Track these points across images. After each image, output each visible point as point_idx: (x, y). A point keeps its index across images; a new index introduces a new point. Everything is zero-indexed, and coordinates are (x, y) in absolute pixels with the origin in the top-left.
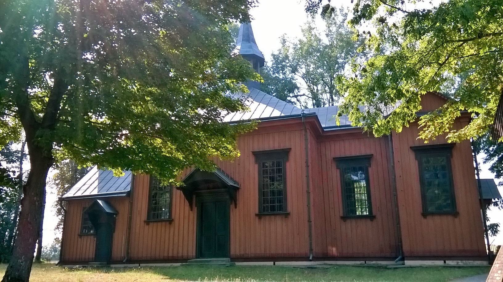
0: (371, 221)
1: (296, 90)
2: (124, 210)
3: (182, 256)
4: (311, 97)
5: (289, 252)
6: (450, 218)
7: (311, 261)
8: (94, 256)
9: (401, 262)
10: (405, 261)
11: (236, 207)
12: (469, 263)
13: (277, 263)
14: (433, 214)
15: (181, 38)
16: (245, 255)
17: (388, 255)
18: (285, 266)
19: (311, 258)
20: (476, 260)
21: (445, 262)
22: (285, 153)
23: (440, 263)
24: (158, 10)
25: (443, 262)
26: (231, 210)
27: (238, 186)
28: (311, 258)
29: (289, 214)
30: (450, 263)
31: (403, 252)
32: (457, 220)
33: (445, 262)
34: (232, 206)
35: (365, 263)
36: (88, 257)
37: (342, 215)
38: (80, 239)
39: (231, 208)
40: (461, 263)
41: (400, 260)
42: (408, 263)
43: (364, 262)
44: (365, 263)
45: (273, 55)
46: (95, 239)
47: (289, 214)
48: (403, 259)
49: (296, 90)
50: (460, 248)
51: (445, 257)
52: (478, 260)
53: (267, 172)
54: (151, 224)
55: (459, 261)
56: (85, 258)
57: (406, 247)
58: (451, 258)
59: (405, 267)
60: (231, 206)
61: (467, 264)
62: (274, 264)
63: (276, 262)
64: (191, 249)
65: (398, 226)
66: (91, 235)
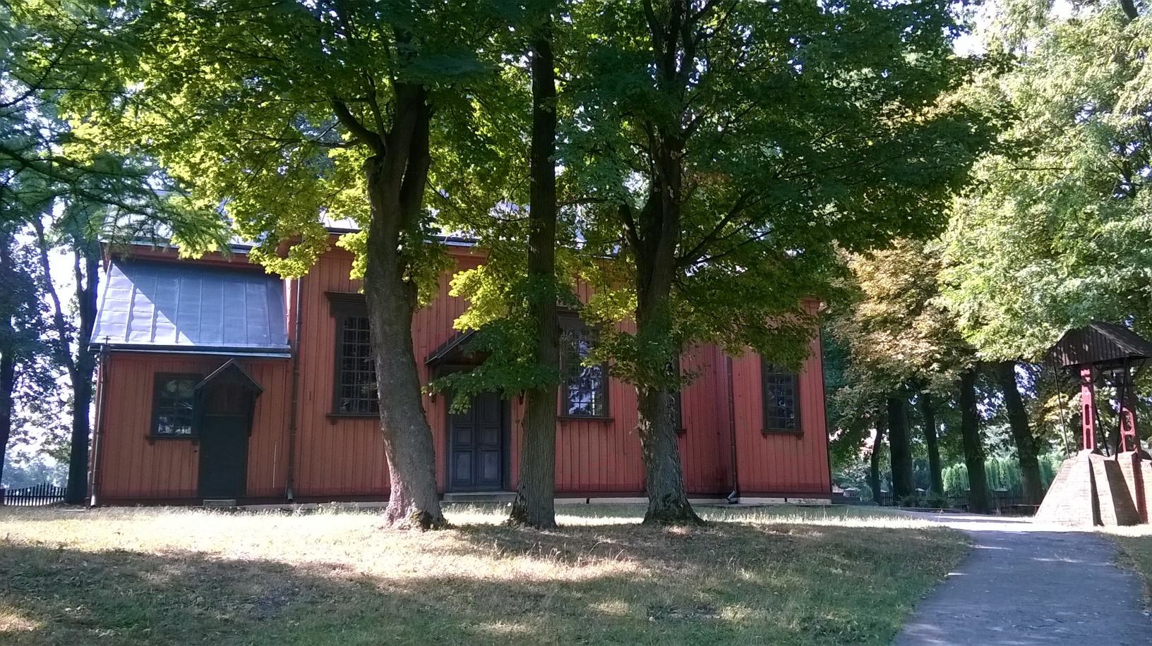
2: (274, 389)
4: (24, 89)
6: (793, 439)
8: (195, 487)
10: (741, 499)
13: (591, 500)
17: (699, 490)
19: (290, 497)
21: (786, 500)
23: (781, 501)
24: (778, 133)
25: (784, 499)
26: (513, 407)
28: (93, 503)
30: (790, 500)
32: (800, 443)
33: (786, 500)
38: (149, 447)
42: (744, 501)
46: (197, 448)
48: (738, 495)
51: (787, 493)
54: (341, 423)
56: (169, 491)
57: (742, 478)
58: (794, 494)
63: (591, 500)
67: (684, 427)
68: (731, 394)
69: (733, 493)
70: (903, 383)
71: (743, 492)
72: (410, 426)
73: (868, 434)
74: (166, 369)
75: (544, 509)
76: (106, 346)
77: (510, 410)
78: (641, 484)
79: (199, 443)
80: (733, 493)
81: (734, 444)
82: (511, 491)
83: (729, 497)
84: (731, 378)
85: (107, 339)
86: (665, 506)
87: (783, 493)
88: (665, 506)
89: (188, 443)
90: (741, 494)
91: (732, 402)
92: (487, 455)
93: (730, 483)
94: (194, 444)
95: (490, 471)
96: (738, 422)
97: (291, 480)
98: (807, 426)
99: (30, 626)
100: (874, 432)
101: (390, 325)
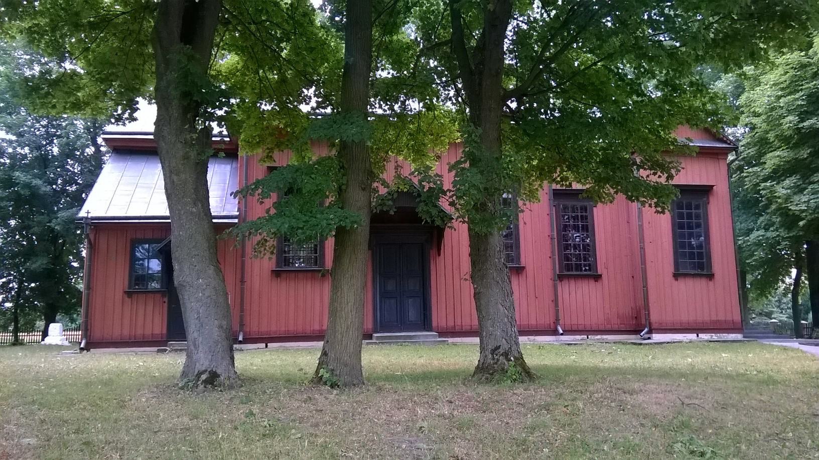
3: (144, 335)
5: (727, 319)
8: (165, 331)
10: (654, 335)
11: (439, 255)
12: (724, 336)
17: (616, 327)
19: (241, 338)
20: (730, 333)
21: (698, 336)
22: (705, 191)
23: (693, 336)
25: (696, 335)
28: (241, 338)
30: (704, 336)
31: (650, 324)
32: (711, 283)
33: (698, 336)
34: (433, 252)
36: (151, 333)
38: (126, 299)
39: (431, 253)
40: (715, 337)
42: (657, 337)
43: (586, 336)
44: (588, 338)
46: (166, 300)
48: (650, 332)
50: (714, 318)
52: (733, 333)
55: (713, 335)
56: (144, 335)
57: (654, 317)
59: (651, 344)
60: (431, 251)
61: (721, 338)
62: (266, 346)
63: (268, 344)
65: (645, 288)
66: (154, 292)
67: (599, 273)
68: (642, 240)
69: (646, 330)
70: (273, 74)
71: (654, 329)
72: (198, 279)
73: (788, 274)
74: (139, 235)
75: (346, 365)
76: (87, 218)
77: (430, 263)
78: (552, 323)
79: (167, 295)
80: (646, 330)
81: (645, 286)
82: (431, 331)
83: (642, 334)
84: (641, 227)
85: (88, 213)
86: (493, 359)
87: (695, 329)
88: (493, 359)
89: (158, 296)
90: (653, 331)
91: (643, 249)
92: (410, 300)
93: (643, 321)
94: (163, 296)
95: (413, 314)
96: (649, 264)
97: (242, 325)
98: (717, 268)
99: (811, 312)
100: (794, 272)
101: (177, 175)
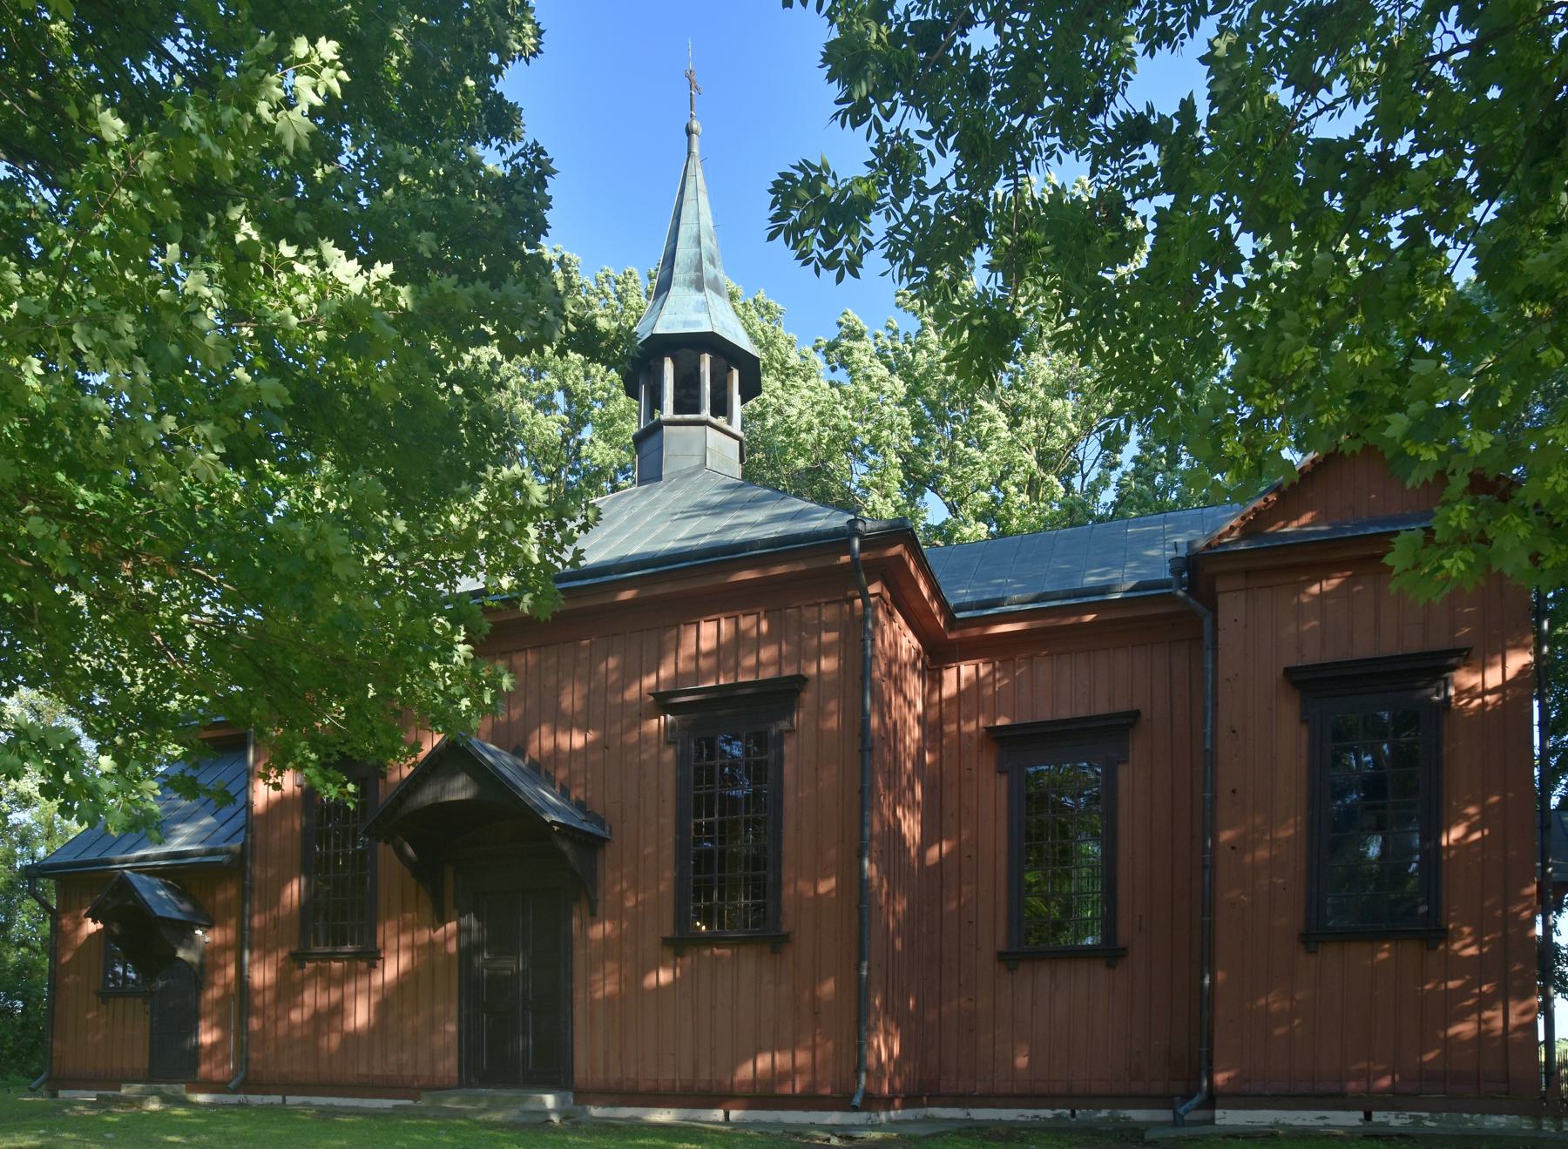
0: (1110, 966)
1: (232, 892)
7: (855, 1109)
8: (147, 1066)
9: (1202, 1114)
10: (1218, 1113)
14: (1343, 937)
15: (127, 674)
16: (678, 1084)
18: (1340, 1132)
27: (600, 832)
28: (857, 1101)
29: (786, 939)
33: (1368, 1116)
35: (1073, 1114)
37: (1002, 946)
41: (1199, 1107)
43: (1068, 1112)
45: (983, 49)
47: (786, 939)
49: (232, 892)
53: (711, 780)
64: (449, 1065)
